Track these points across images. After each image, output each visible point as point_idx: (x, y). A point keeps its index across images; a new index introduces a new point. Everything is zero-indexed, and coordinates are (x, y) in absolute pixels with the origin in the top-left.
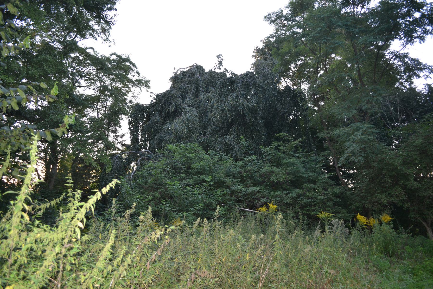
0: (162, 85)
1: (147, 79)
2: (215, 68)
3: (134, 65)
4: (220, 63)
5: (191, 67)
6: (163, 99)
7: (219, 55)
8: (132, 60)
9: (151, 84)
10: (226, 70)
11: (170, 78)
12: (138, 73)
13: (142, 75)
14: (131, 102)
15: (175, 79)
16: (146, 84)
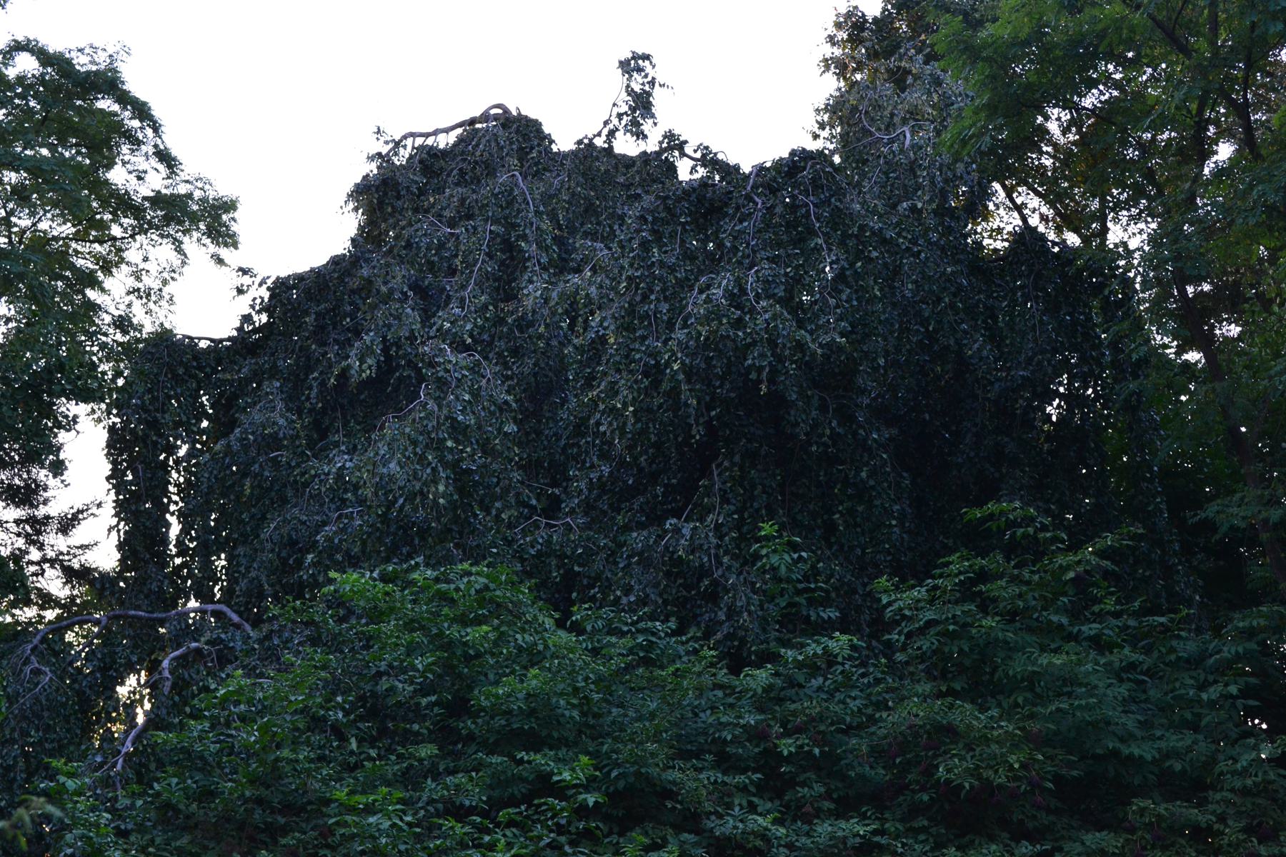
0: (298, 225)
1: (222, 189)
2: (612, 134)
3: (142, 111)
4: (642, 104)
5: (472, 122)
6: (304, 308)
7: (636, 57)
8: (135, 85)
9: (241, 223)
10: (674, 143)
11: (349, 187)
12: (165, 157)
13: (189, 168)
14: (123, 323)
15: (381, 195)
16: (213, 219)
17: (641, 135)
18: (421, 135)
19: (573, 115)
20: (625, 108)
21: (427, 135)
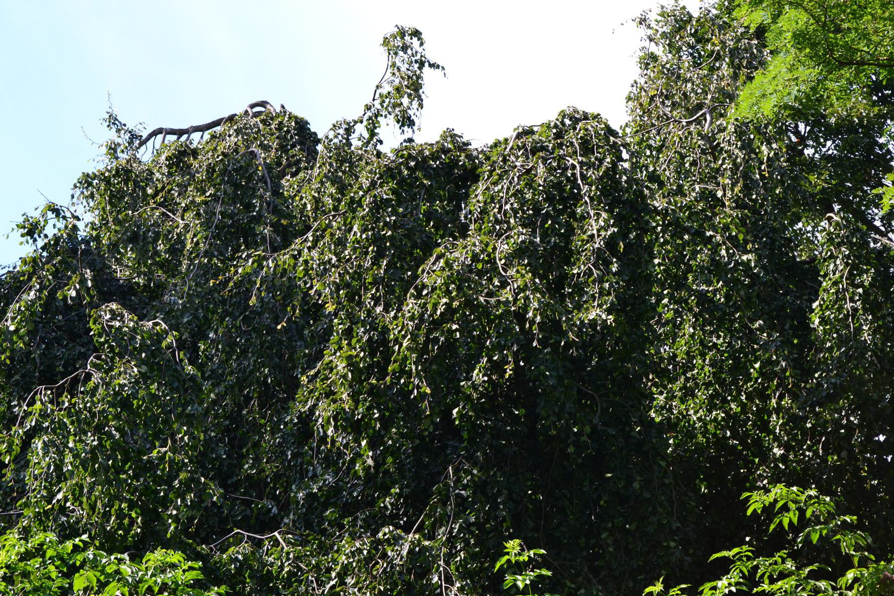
4: (407, 91)
5: (231, 119)
15: (118, 186)
17: (406, 121)
18: (172, 132)
19: (331, 96)
20: (387, 88)
21: (180, 133)
